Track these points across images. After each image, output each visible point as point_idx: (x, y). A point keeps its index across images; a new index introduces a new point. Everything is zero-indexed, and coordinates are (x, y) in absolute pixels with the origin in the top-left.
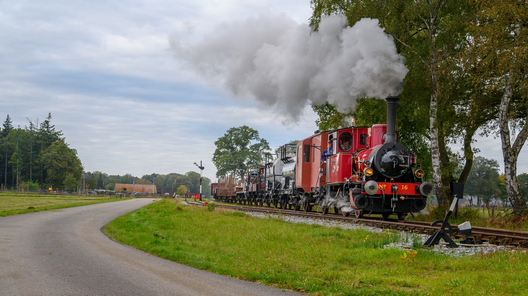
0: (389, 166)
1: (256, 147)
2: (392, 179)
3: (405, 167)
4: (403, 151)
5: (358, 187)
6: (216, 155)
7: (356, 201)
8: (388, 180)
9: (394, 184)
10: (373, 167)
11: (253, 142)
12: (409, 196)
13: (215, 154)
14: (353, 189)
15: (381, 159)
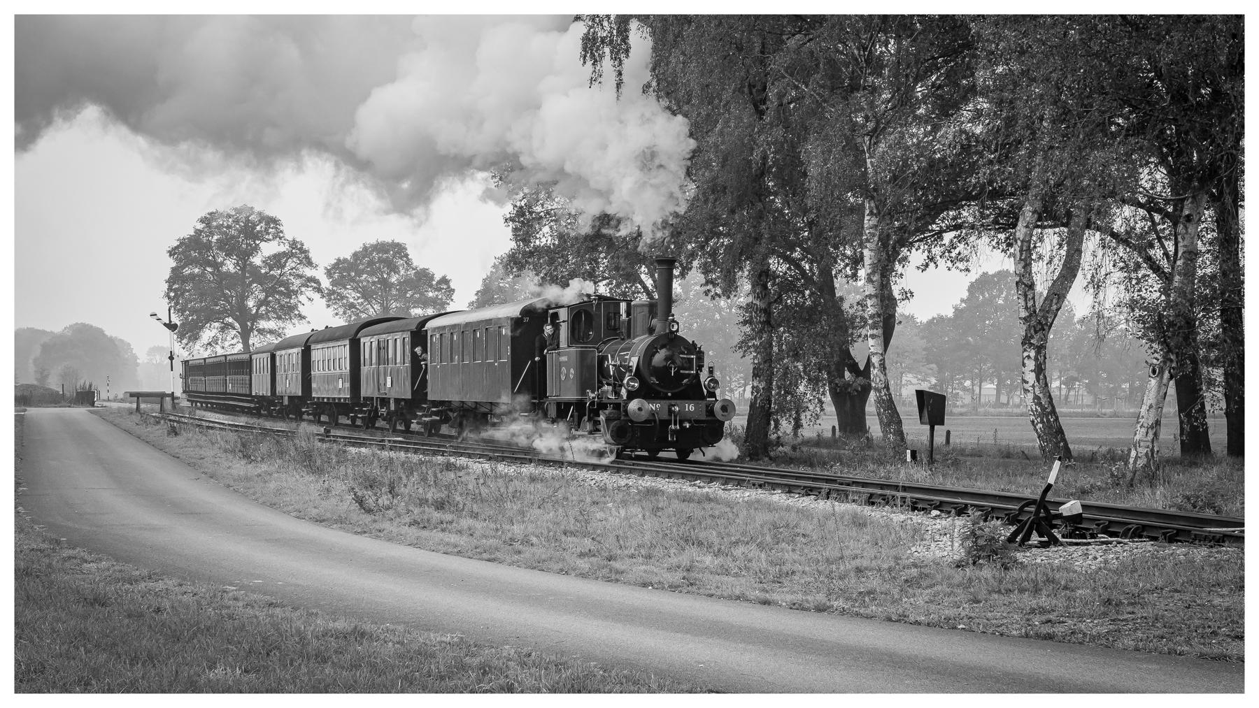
0: (662, 372)
1: (277, 261)
2: (669, 394)
3: (690, 374)
4: (685, 348)
5: (614, 408)
6: (174, 283)
7: (612, 431)
8: (666, 398)
9: (673, 402)
10: (638, 374)
11: (269, 248)
12: (697, 421)
13: (171, 281)
14: (607, 412)
15: (651, 360)
